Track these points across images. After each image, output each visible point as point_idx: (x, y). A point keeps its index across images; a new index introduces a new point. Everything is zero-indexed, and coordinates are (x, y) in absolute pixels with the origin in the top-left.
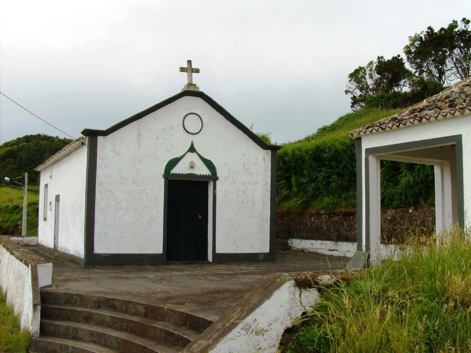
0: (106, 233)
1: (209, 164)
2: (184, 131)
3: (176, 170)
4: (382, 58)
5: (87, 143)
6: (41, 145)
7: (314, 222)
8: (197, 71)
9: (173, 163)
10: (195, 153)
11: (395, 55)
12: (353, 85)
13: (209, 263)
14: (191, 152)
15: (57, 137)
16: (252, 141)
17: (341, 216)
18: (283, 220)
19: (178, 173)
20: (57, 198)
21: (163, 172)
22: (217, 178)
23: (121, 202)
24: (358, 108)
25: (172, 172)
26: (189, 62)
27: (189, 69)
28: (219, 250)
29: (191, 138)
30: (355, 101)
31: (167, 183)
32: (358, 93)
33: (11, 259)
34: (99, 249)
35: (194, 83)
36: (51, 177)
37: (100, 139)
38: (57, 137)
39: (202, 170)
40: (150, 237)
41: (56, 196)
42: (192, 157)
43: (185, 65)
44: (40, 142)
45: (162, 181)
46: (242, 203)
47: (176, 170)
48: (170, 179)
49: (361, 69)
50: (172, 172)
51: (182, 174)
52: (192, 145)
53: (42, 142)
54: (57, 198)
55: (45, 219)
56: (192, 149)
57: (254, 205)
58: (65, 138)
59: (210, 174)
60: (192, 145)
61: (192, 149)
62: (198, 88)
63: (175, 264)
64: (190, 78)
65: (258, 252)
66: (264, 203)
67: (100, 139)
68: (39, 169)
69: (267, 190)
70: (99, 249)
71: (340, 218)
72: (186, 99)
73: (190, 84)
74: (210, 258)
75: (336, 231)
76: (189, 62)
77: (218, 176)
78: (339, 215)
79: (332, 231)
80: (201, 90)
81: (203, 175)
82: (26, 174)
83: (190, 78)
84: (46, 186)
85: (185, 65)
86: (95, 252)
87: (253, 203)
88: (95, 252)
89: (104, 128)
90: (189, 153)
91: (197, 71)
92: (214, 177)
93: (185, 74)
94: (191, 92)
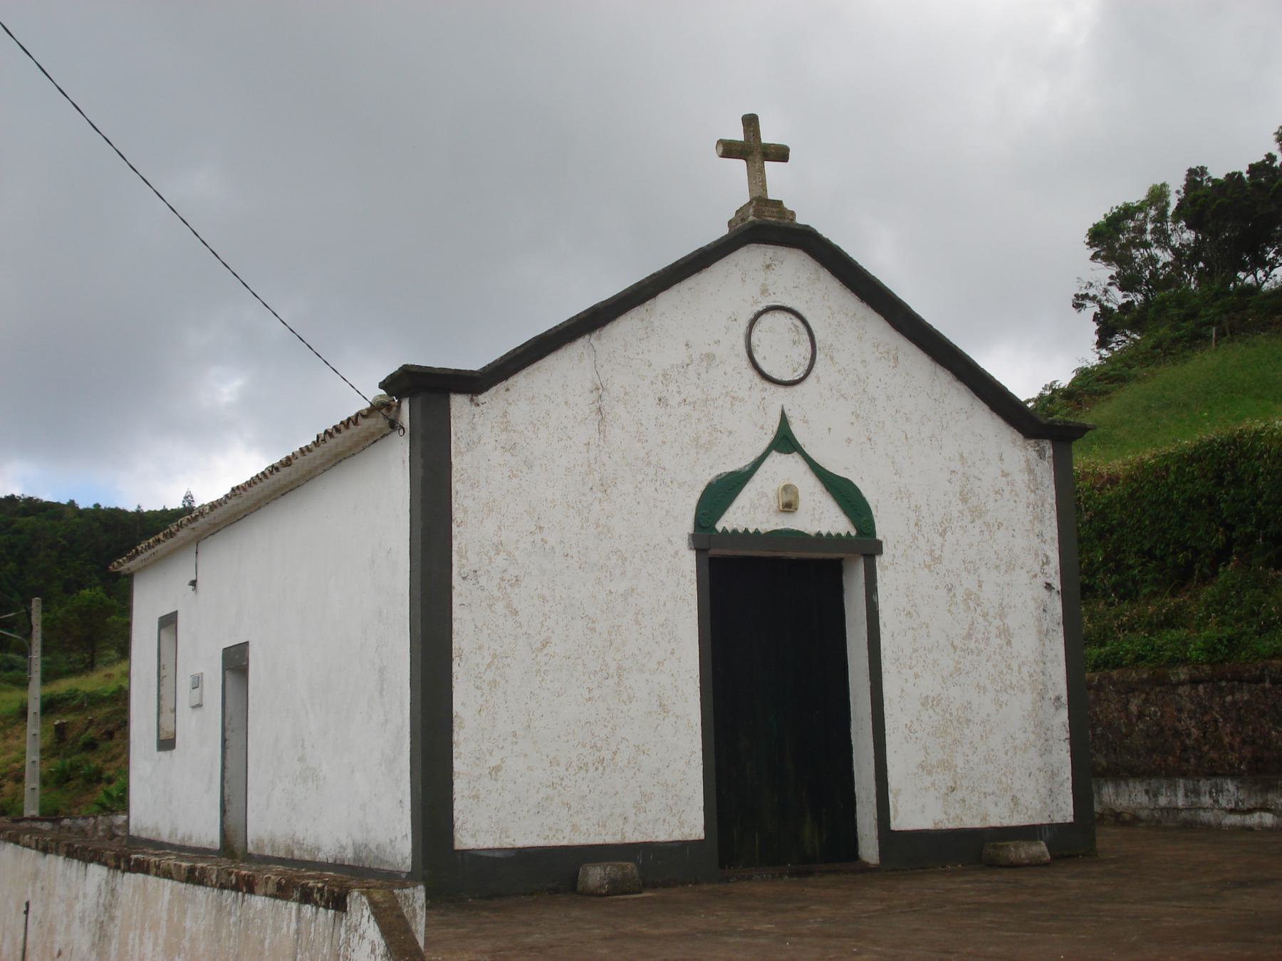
0: (497, 769)
1: (844, 493)
2: (750, 373)
3: (738, 517)
4: (1203, 170)
5: (406, 424)
6: (19, 531)
7: (1141, 716)
8: (781, 154)
9: (723, 491)
10: (795, 454)
11: (1259, 158)
12: (1104, 272)
13: (867, 869)
14: (781, 451)
15: (72, 503)
16: (985, 407)
17: (1267, 685)
18: (1185, 602)
19: (824, 532)
20: (236, 662)
21: (687, 525)
22: (877, 548)
23: (545, 644)
24: (1119, 342)
25: (719, 527)
26: (751, 122)
27: (752, 149)
28: (905, 817)
29: (780, 397)
30: (1108, 325)
31: (706, 568)
32: (1117, 298)
33: (150, 888)
34: (480, 826)
35: (772, 195)
36: (194, 583)
37: (459, 404)
38: (72, 503)
39: (822, 518)
40: (656, 784)
41: (227, 652)
42: (784, 468)
43: (738, 135)
44: (13, 522)
45: (689, 561)
46: (969, 636)
47: (738, 517)
48: (715, 552)
49: (1127, 212)
50: (719, 527)
51: (757, 532)
52: (784, 420)
53: (21, 521)
54: (236, 662)
55: (167, 744)
56: (785, 441)
57: (1009, 643)
58: (97, 506)
59: (853, 533)
60: (784, 420)
61: (785, 441)
62: (793, 213)
63: (750, 878)
64: (757, 178)
65: (1037, 821)
66: (1044, 634)
67: (459, 404)
68: (125, 566)
69: (1049, 586)
70: (480, 826)
71: (1264, 690)
72: (751, 257)
73: (761, 202)
74: (869, 849)
75: (1244, 742)
76: (751, 122)
77: (879, 537)
78: (1260, 680)
79: (1227, 740)
80: (801, 220)
81: (829, 534)
82: (36, 603)
83: (757, 178)
84: (169, 622)
85: (738, 135)
86: (457, 846)
87: (1005, 633)
88: (457, 846)
89: (475, 362)
90: (774, 454)
91: (781, 154)
92: (866, 544)
93: (740, 165)
94: (766, 227)
